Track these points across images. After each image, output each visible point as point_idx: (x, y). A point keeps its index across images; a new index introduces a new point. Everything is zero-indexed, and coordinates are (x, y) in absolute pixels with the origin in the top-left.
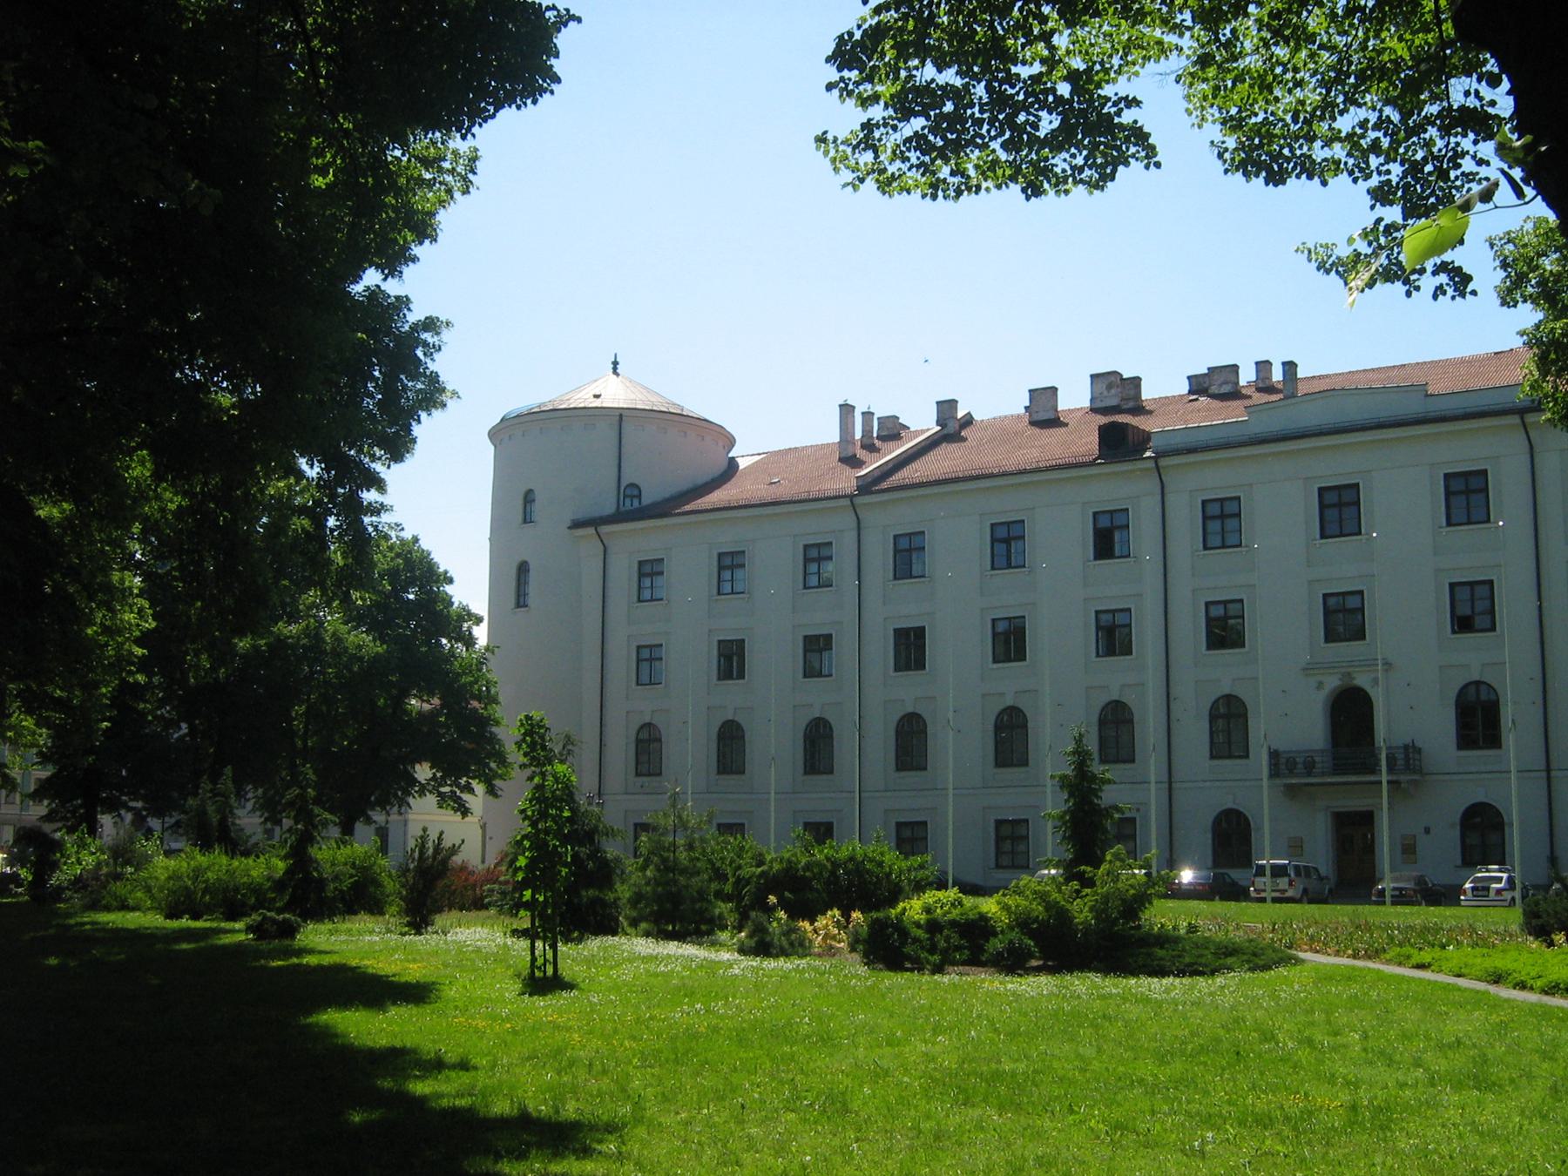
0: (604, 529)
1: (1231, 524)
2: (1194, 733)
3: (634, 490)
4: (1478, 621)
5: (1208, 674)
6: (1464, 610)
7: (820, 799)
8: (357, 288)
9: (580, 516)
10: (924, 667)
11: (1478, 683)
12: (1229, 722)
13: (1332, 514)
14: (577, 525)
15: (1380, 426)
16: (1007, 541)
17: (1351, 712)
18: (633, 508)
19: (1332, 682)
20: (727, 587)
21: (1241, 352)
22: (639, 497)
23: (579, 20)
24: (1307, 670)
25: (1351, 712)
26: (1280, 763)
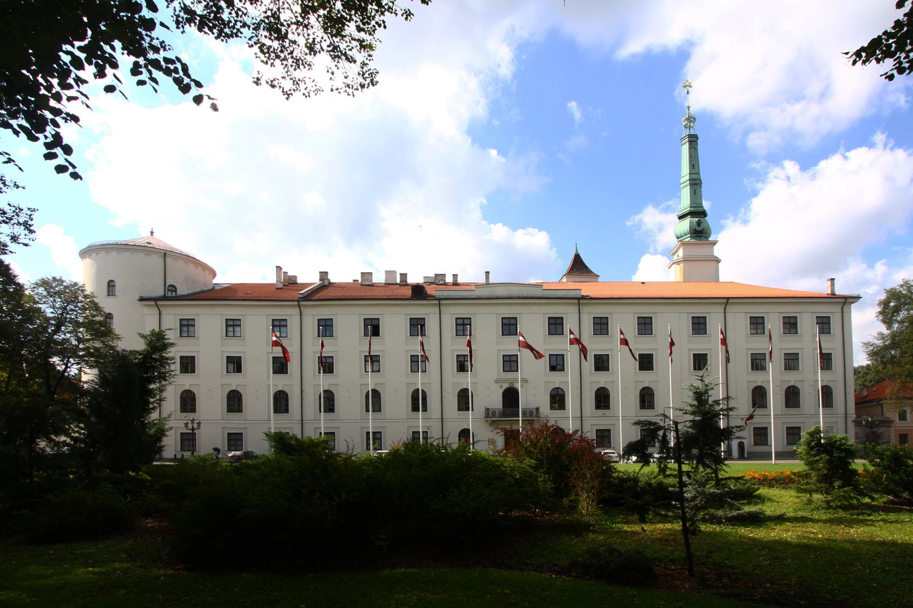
0: (160, 303)
1: (191, 329)
2: (452, 402)
3: (173, 288)
4: (559, 367)
5: (456, 381)
6: (554, 364)
7: (235, 423)
8: (629, 223)
9: (145, 295)
10: (332, 372)
11: (557, 388)
12: (464, 400)
13: (506, 327)
14: (142, 299)
15: (519, 298)
16: (464, 325)
17: (511, 396)
18: (170, 296)
19: (506, 386)
20: (231, 334)
21: (638, 272)
22: (176, 291)
23: (287, 99)
24: (496, 381)
25: (511, 396)
26: (488, 413)
